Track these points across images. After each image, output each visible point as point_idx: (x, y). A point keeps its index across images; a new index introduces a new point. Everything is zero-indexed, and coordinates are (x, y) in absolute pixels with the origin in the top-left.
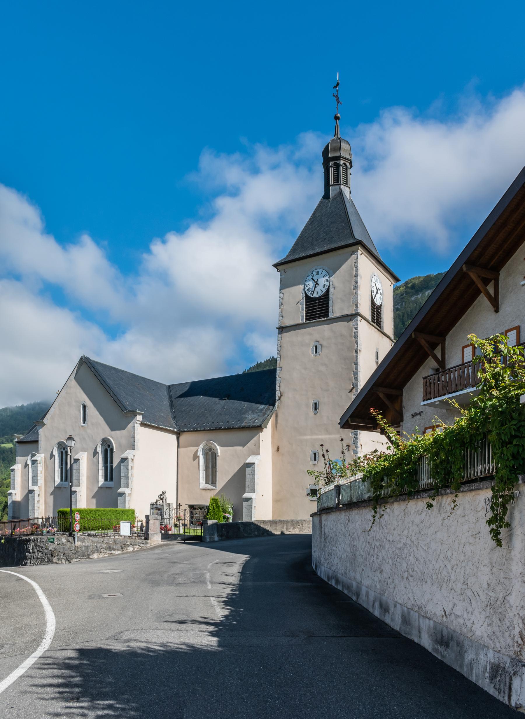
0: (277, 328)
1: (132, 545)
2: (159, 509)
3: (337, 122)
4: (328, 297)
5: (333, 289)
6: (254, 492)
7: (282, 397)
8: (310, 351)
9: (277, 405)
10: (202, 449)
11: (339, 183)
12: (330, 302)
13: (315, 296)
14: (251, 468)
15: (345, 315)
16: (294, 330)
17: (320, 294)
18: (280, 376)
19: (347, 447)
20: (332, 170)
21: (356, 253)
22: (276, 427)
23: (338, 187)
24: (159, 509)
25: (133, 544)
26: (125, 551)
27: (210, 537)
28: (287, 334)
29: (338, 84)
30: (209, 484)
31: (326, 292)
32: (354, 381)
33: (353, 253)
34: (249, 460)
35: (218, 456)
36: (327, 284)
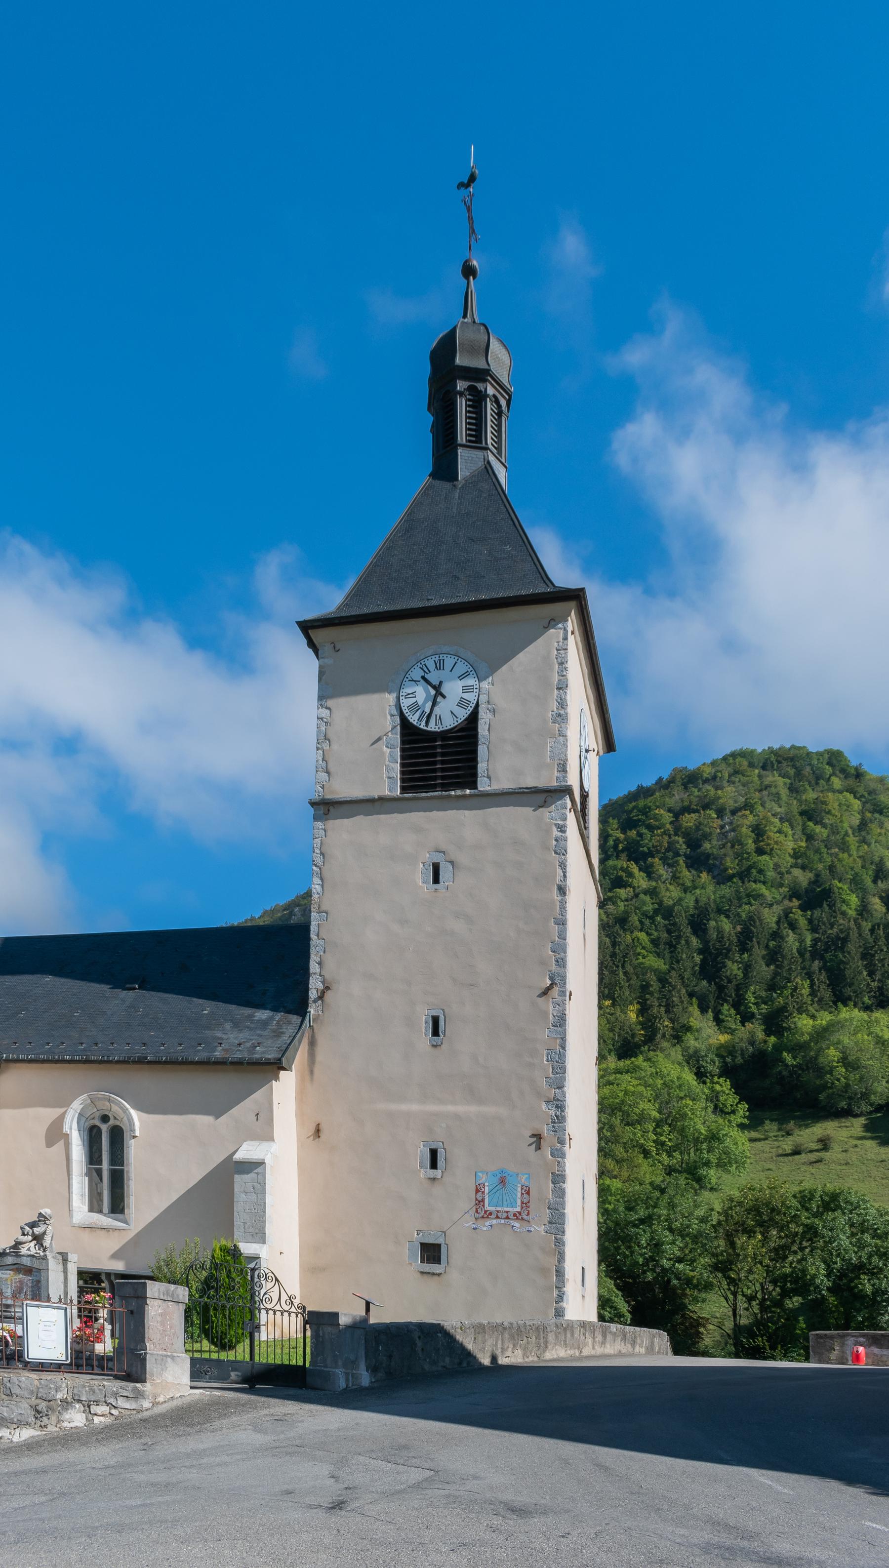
0: (313, 804)
1: (79, 1401)
2: (28, 1271)
3: (468, 283)
4: (475, 736)
5: (490, 715)
6: (264, 1242)
7: (328, 994)
8: (420, 876)
9: (312, 1012)
10: (77, 1116)
11: (481, 443)
12: (482, 750)
13: (433, 727)
14: (252, 1175)
15: (527, 788)
16: (367, 814)
17: (449, 723)
18: (322, 935)
19: (534, 1139)
20: (462, 406)
21: (560, 625)
22: (312, 1072)
23: (480, 454)
24: (28, 1271)
25: (84, 1398)
26: (52, 1429)
27: (347, 1374)
28: (346, 821)
29: (472, 178)
30: (100, 1211)
31: (466, 720)
32: (554, 968)
33: (551, 623)
34: (247, 1152)
35: (134, 1137)
36: (471, 697)
